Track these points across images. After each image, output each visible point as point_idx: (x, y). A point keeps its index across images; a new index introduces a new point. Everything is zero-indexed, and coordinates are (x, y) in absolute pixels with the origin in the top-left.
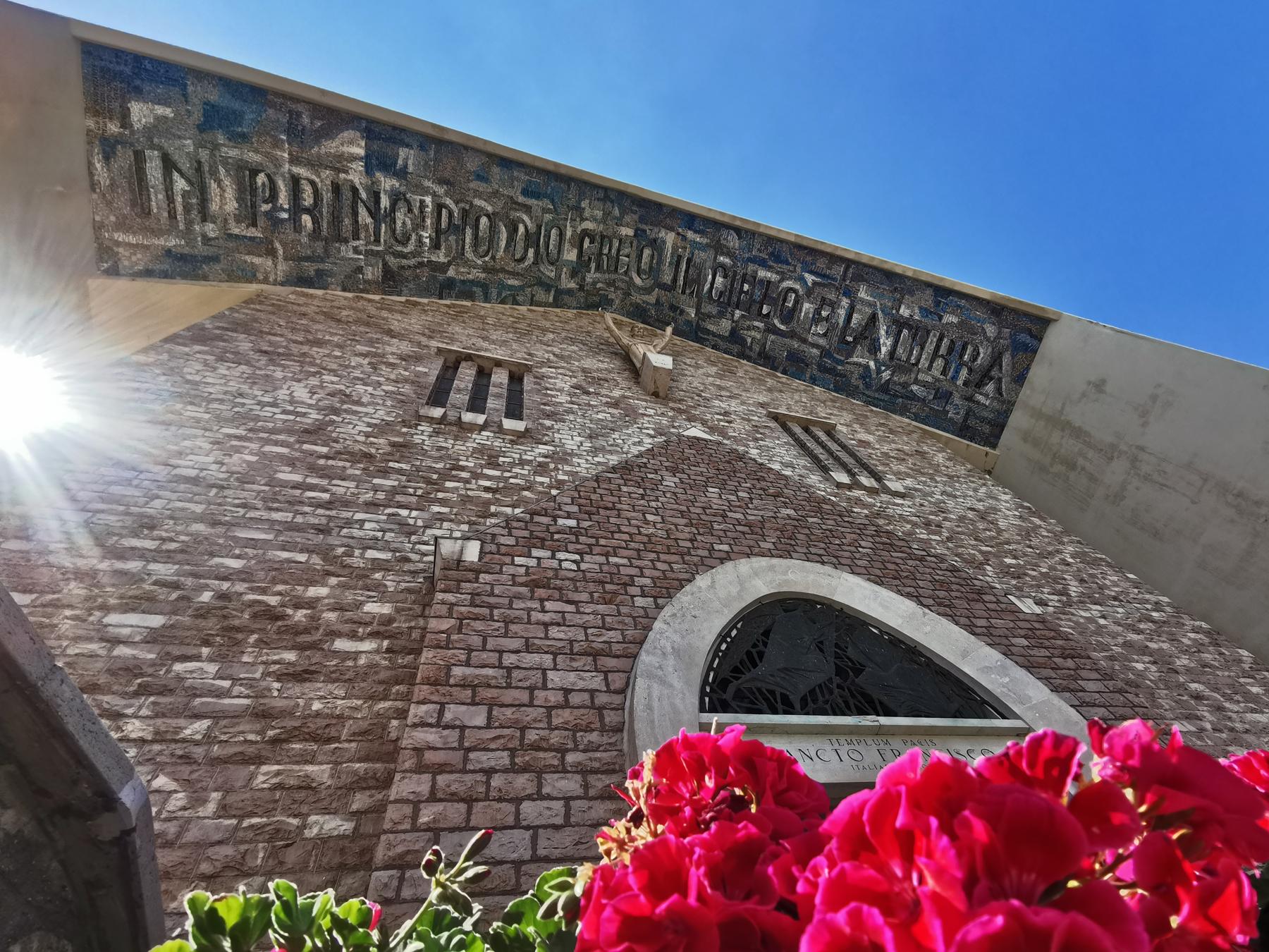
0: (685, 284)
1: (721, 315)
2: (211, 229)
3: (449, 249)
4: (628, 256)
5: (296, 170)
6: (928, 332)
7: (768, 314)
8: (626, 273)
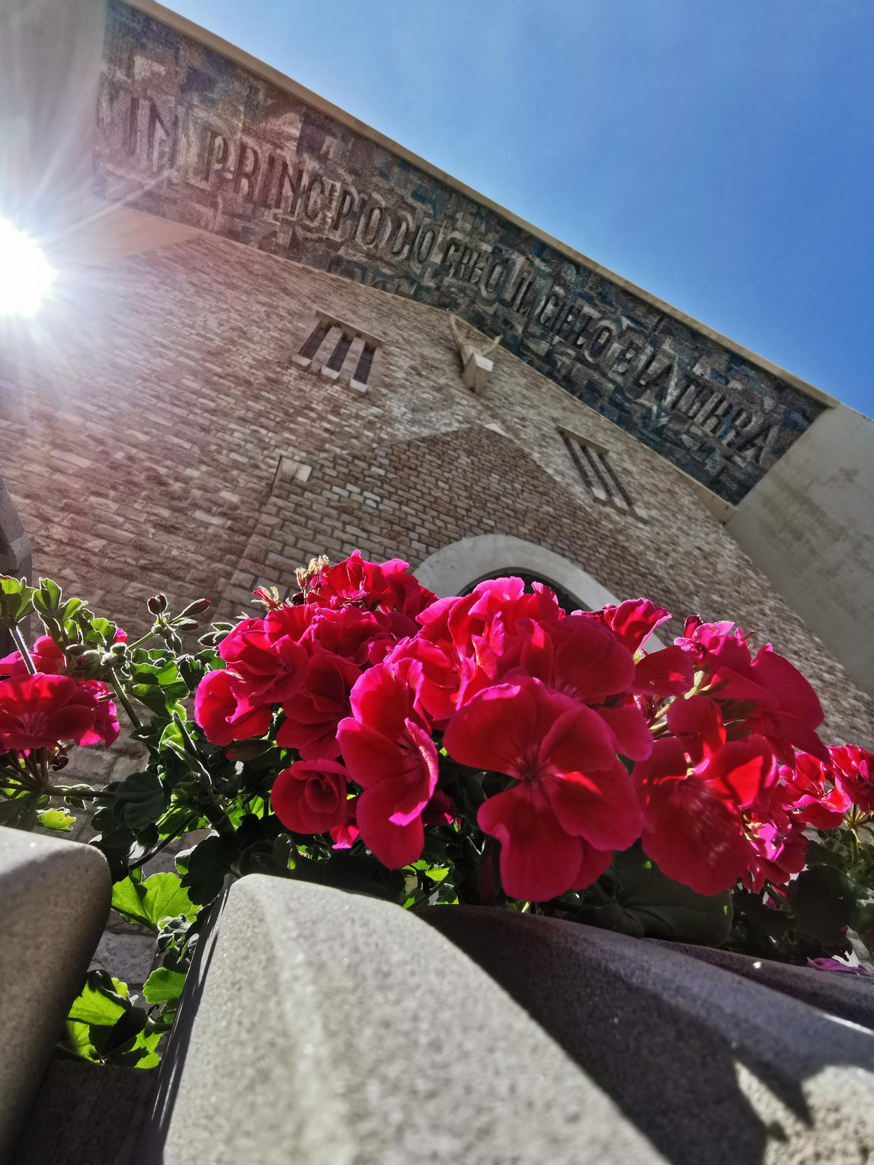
0: (521, 304)
1: (543, 337)
4: (482, 269)
7: (581, 346)
8: (476, 283)
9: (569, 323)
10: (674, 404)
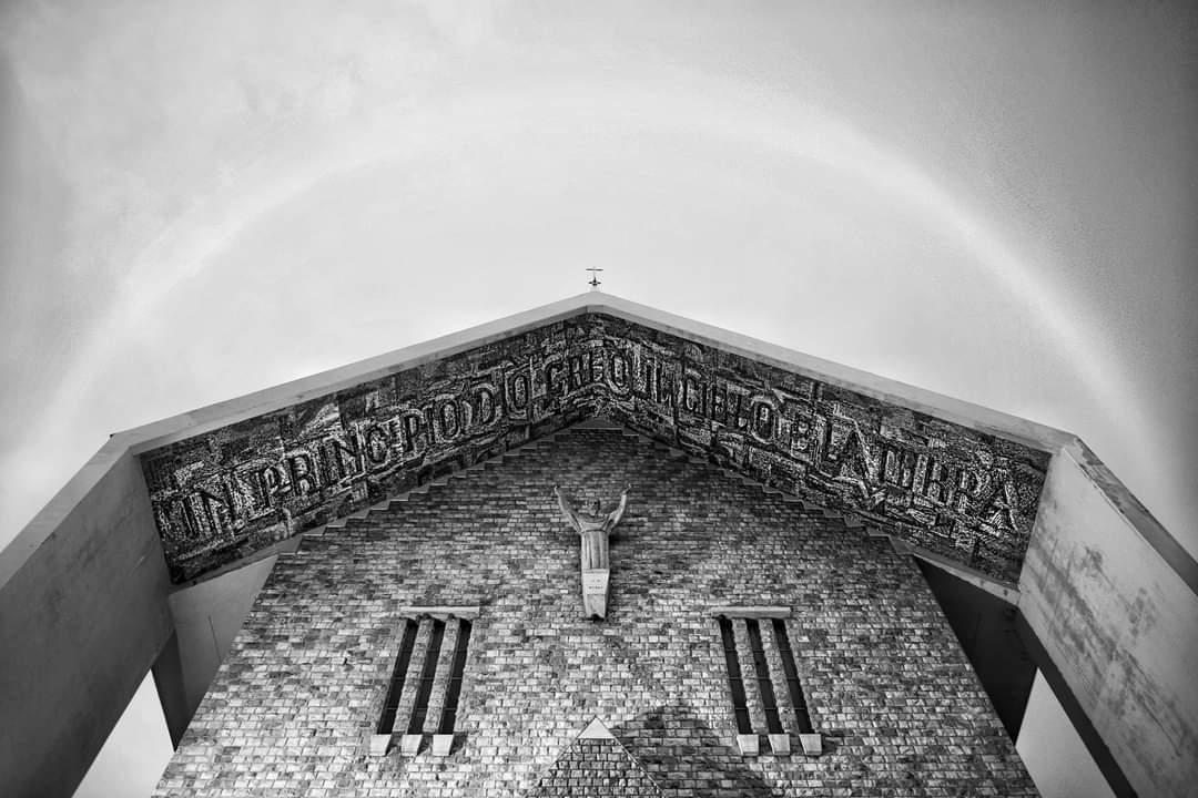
0: (659, 393)
1: (699, 425)
2: (239, 524)
3: (421, 445)
4: (601, 364)
5: (290, 455)
6: (916, 456)
7: (745, 428)
8: (602, 380)
9: (720, 405)
10: (881, 475)
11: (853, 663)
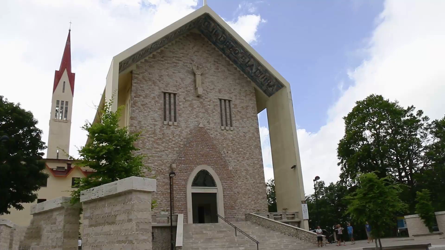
11: (240, 112)
